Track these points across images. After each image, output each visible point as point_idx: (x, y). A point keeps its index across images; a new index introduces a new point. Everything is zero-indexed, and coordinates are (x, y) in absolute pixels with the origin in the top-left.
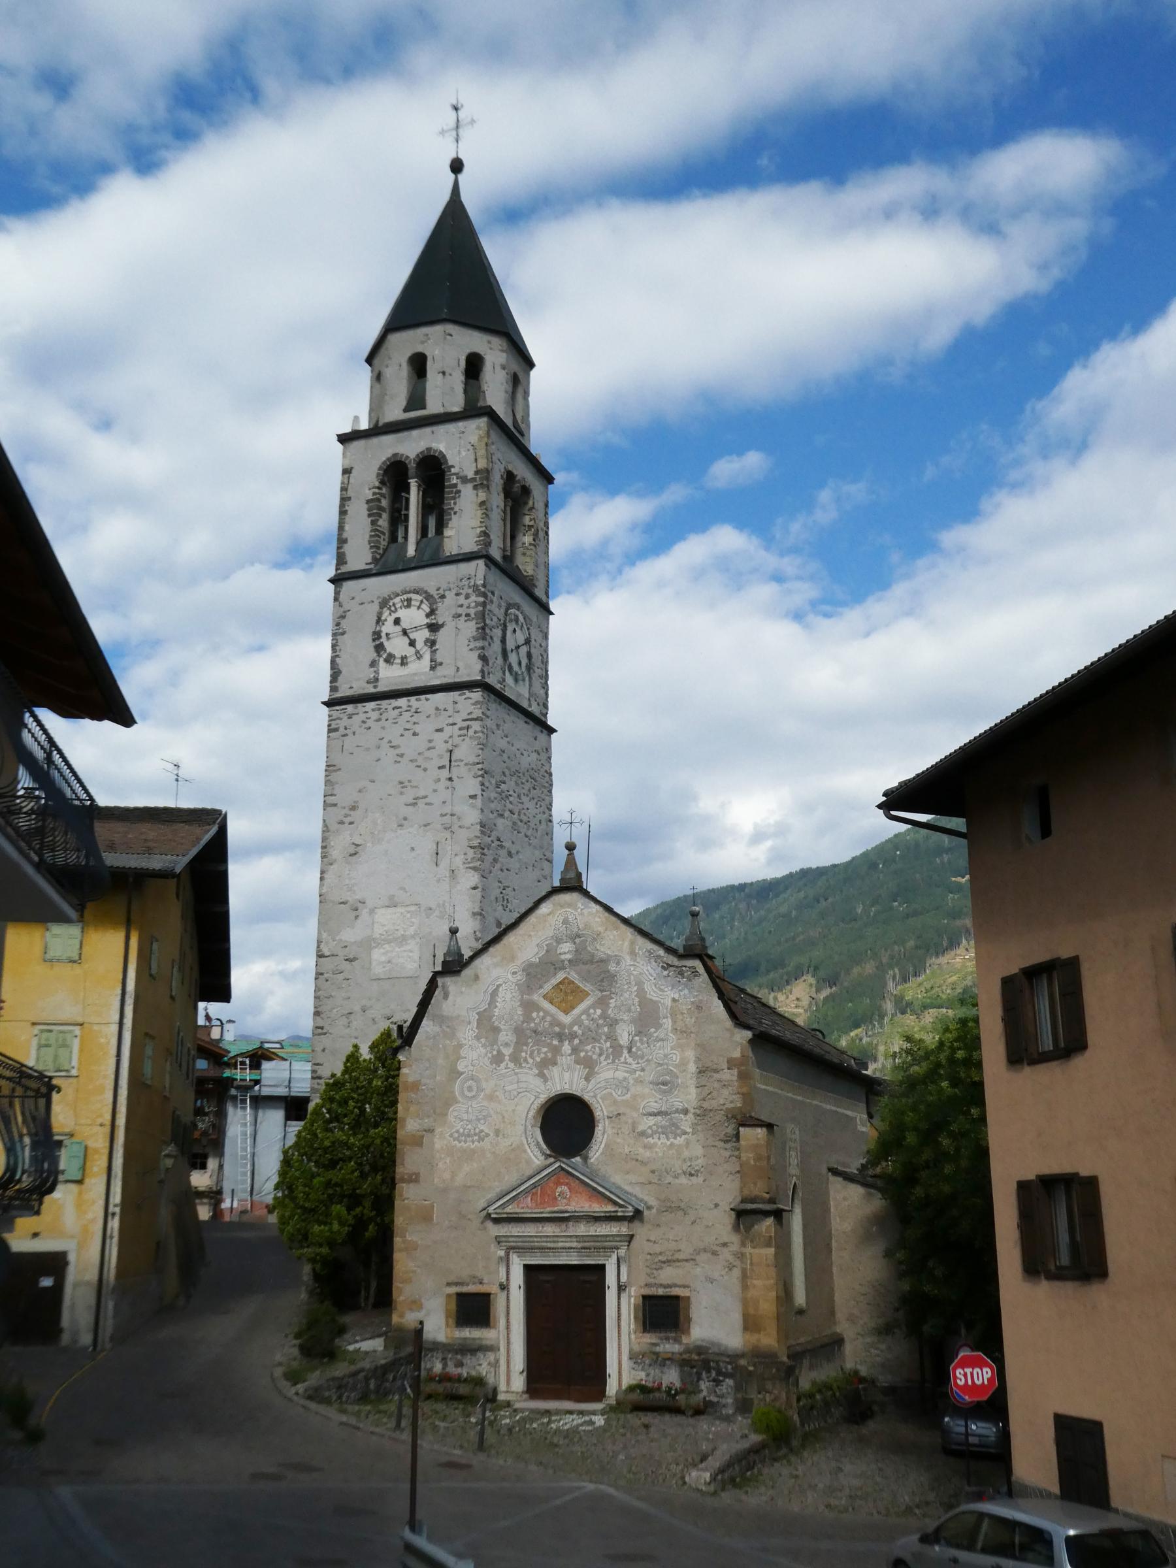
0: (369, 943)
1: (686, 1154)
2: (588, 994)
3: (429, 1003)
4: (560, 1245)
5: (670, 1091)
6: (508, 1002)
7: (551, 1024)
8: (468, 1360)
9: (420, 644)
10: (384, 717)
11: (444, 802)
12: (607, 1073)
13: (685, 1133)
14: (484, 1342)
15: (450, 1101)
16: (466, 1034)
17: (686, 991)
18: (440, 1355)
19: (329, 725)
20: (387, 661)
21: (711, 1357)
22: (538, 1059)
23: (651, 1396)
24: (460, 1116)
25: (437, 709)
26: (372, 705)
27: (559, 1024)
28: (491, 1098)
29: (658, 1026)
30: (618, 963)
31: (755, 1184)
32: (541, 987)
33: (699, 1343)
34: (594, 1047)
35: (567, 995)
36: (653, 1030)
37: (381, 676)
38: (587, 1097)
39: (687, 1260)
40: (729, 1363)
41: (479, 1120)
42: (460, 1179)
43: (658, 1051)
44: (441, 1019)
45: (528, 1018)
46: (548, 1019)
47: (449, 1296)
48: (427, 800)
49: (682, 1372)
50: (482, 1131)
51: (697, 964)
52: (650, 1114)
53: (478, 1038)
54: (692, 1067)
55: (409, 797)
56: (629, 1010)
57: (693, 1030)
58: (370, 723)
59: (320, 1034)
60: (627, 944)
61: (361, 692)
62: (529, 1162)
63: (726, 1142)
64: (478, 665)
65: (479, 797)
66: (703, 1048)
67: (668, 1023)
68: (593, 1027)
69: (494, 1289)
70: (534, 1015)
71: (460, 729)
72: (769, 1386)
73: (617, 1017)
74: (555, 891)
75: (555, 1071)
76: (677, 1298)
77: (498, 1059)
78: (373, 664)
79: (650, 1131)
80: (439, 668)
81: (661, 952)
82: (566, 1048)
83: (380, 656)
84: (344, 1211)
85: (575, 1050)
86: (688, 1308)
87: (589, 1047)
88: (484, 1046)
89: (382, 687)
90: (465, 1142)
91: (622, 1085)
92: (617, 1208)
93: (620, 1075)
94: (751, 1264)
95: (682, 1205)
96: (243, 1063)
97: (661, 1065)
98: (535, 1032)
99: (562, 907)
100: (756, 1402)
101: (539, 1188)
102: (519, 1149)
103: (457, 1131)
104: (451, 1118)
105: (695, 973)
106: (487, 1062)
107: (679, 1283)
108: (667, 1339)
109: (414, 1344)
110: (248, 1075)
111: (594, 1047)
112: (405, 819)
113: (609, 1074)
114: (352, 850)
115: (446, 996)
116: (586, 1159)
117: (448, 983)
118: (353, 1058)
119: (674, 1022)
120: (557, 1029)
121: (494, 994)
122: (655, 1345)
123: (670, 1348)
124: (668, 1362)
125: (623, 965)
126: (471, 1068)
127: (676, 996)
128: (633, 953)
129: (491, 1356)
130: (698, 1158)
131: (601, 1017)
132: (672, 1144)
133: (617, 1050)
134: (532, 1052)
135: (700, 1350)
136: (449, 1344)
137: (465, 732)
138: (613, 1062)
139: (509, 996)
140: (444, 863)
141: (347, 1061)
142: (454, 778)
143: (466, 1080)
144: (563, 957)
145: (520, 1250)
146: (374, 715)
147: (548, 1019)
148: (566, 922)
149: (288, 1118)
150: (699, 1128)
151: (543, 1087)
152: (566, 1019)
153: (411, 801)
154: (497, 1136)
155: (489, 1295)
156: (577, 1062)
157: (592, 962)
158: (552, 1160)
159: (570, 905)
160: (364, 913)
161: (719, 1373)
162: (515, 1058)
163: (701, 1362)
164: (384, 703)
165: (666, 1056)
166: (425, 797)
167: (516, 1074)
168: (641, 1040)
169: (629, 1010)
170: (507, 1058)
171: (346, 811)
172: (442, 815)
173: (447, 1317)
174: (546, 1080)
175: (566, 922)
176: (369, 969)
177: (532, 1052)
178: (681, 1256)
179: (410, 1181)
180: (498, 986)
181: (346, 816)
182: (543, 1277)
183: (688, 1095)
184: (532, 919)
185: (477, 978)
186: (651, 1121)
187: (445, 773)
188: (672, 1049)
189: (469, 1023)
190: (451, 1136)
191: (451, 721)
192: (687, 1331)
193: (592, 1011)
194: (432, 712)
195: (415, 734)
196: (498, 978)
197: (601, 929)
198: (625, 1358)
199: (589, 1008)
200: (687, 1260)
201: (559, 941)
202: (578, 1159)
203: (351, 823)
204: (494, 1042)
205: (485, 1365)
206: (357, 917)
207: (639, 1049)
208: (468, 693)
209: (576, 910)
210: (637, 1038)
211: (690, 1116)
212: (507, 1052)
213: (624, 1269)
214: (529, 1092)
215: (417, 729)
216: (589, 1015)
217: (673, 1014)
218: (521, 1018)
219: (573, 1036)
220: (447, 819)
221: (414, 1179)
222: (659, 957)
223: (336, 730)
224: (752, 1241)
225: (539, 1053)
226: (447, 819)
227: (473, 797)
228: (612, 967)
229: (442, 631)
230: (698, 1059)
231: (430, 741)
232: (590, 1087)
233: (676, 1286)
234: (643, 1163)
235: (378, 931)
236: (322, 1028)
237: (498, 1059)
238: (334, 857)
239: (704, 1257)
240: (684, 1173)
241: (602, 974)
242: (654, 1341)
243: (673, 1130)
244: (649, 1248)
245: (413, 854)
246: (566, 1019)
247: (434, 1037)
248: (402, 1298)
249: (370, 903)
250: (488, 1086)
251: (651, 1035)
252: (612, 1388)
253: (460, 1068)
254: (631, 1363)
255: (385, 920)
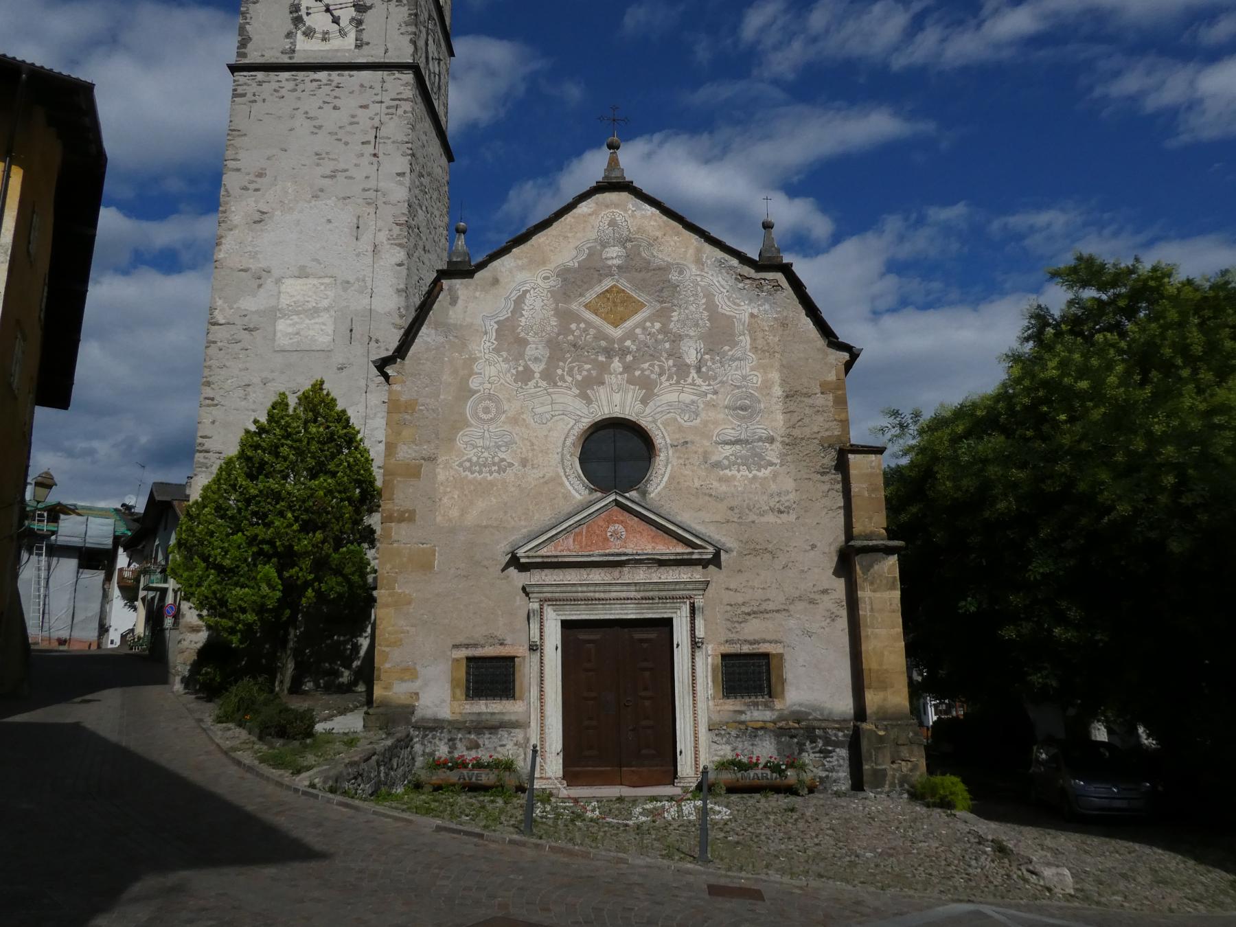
0: (273, 314)
1: (773, 487)
2: (643, 305)
3: (430, 308)
4: (613, 595)
5: (751, 417)
6: (538, 310)
7: (595, 338)
8: (486, 740)
9: (344, 22)
10: (301, 87)
11: (367, 177)
12: (669, 395)
13: (771, 464)
14: (506, 718)
15: (459, 423)
16: (483, 346)
17: (767, 307)
18: (446, 735)
19: (235, 90)
20: (305, 34)
21: (816, 724)
22: (579, 378)
23: (752, 773)
24: (473, 442)
25: (362, 86)
26: (287, 75)
27: (606, 337)
28: (515, 421)
29: (734, 344)
30: (681, 272)
31: (870, 518)
32: (581, 295)
33: (796, 708)
34: (652, 365)
35: (616, 306)
36: (727, 348)
37: (298, 48)
38: (644, 423)
39: (778, 611)
40: (839, 729)
41: (499, 447)
42: (472, 517)
43: (734, 373)
44: (445, 328)
45: (565, 330)
46: (592, 331)
47: (457, 660)
48: (347, 174)
49: (779, 743)
50: (503, 460)
51: (779, 277)
52: (726, 443)
53: (497, 351)
54: (777, 391)
55: (327, 167)
56: (697, 325)
57: (777, 348)
58: (283, 92)
59: (208, 406)
60: (691, 252)
61: (273, 60)
62: (567, 496)
63: (823, 474)
64: (411, 49)
65: (408, 174)
66: (788, 369)
67: (746, 340)
68: (650, 342)
69: (520, 650)
70: (573, 326)
71: (388, 108)
72: (904, 752)
73: (681, 332)
74: (600, 188)
75: (602, 392)
76: (766, 656)
77: (525, 376)
78: (289, 35)
79: (726, 462)
80: (365, 47)
81: (735, 262)
82: (616, 365)
83: (296, 27)
84: (274, 574)
85: (627, 368)
86: (781, 667)
87: (646, 366)
88: (506, 360)
89: (298, 59)
90: (480, 472)
91: (685, 408)
92: (690, 550)
93: (687, 397)
94: (872, 610)
95: (770, 547)
96: (41, 516)
97: (738, 387)
98: (574, 346)
99: (607, 207)
100: (890, 773)
101: (577, 523)
102: (555, 480)
103: (469, 460)
104: (459, 444)
105: (777, 286)
106: (509, 378)
107: (768, 637)
108: (756, 704)
109: (396, 720)
110: (45, 527)
111: (652, 365)
112: (321, 190)
113: (673, 397)
114: (257, 217)
115: (454, 301)
116: (644, 493)
117: (458, 285)
118: (280, 404)
119: (754, 340)
120: (603, 343)
121: (520, 301)
122: (741, 712)
123: (759, 715)
124: (760, 733)
125: (687, 274)
126: (487, 386)
127: (755, 311)
128: (699, 262)
129: (519, 735)
130: (788, 492)
131: (660, 331)
132: (755, 477)
133: (682, 370)
134: (571, 370)
135: (798, 717)
136: (457, 721)
137: (393, 110)
138: (678, 382)
139: (538, 304)
140: (367, 238)
141: (273, 408)
142: (380, 155)
143: (481, 400)
144: (610, 262)
145: (554, 602)
146: (291, 85)
147: (592, 331)
148: (613, 223)
149: (82, 566)
150: (789, 458)
151: (585, 411)
152: (617, 333)
153: (328, 173)
154: (524, 466)
155: (512, 659)
156: (630, 382)
157: (648, 270)
158: (599, 494)
159: (617, 206)
160: (269, 283)
161: (828, 741)
162: (548, 376)
163: (801, 731)
164: (301, 75)
165: (744, 377)
166: (346, 170)
167: (549, 394)
168: (712, 359)
169: (697, 325)
170: (537, 375)
171: (251, 177)
172: (364, 190)
173: (453, 688)
174: (589, 401)
175: (613, 223)
176: (274, 340)
177: (571, 370)
178: (771, 606)
179: (401, 520)
180: (528, 291)
181: (251, 182)
182: (583, 635)
183: (774, 421)
184: (568, 218)
185: (496, 282)
186: (728, 450)
187: (369, 149)
188: (752, 370)
189: (486, 333)
190: (461, 465)
191: (378, 98)
192: (782, 694)
193: (648, 324)
194: (357, 88)
195: (335, 108)
196: (525, 282)
197: (659, 234)
198: (703, 729)
199: (645, 321)
200: (778, 611)
201: (604, 245)
202: (633, 494)
203: (257, 190)
204: (521, 355)
205: (510, 746)
206: (260, 286)
207: (709, 369)
208: (397, 74)
209: (626, 211)
210: (707, 357)
211: (777, 446)
212: (537, 368)
213: (700, 623)
214: (567, 414)
215: (337, 102)
216: (644, 329)
217: (752, 330)
218: (556, 330)
219: (624, 352)
220: (371, 194)
221: (407, 517)
222: (731, 267)
223: (243, 95)
224: (872, 583)
225: (580, 372)
226: (371, 194)
227: (402, 174)
228: (674, 277)
229: (369, 12)
230: (784, 382)
231: (353, 116)
232: (648, 410)
233: (765, 641)
234: (719, 498)
235: (284, 301)
236: (212, 399)
237: (525, 376)
238: (235, 223)
239: (800, 606)
240: (772, 510)
241: (661, 283)
242: (738, 708)
243: (757, 460)
244: (728, 597)
245: (329, 226)
246: (617, 333)
247: (437, 348)
248: (387, 666)
249: (276, 273)
250: (511, 408)
251: (725, 353)
252: (686, 768)
253: (474, 383)
254: (712, 735)
255: (294, 290)
